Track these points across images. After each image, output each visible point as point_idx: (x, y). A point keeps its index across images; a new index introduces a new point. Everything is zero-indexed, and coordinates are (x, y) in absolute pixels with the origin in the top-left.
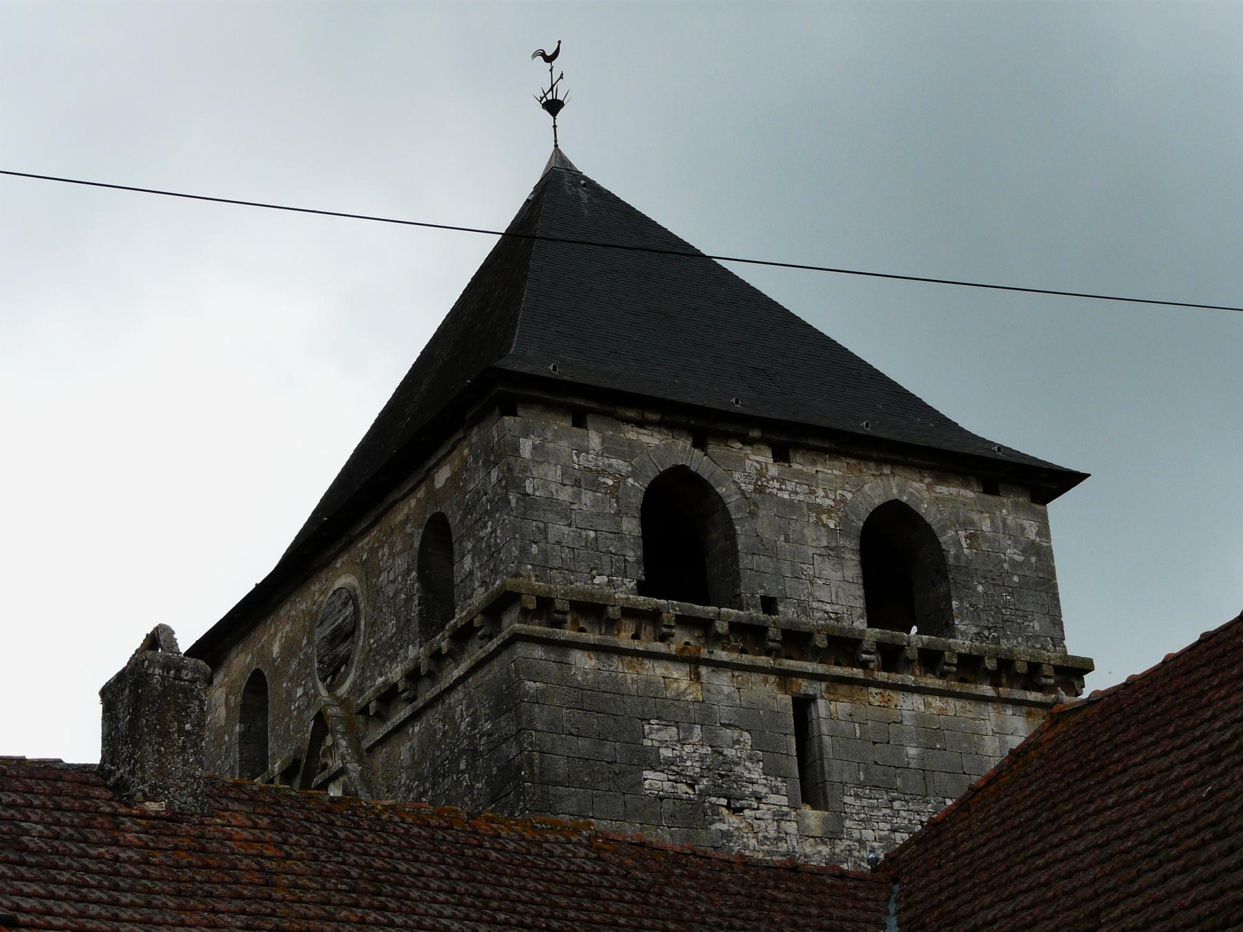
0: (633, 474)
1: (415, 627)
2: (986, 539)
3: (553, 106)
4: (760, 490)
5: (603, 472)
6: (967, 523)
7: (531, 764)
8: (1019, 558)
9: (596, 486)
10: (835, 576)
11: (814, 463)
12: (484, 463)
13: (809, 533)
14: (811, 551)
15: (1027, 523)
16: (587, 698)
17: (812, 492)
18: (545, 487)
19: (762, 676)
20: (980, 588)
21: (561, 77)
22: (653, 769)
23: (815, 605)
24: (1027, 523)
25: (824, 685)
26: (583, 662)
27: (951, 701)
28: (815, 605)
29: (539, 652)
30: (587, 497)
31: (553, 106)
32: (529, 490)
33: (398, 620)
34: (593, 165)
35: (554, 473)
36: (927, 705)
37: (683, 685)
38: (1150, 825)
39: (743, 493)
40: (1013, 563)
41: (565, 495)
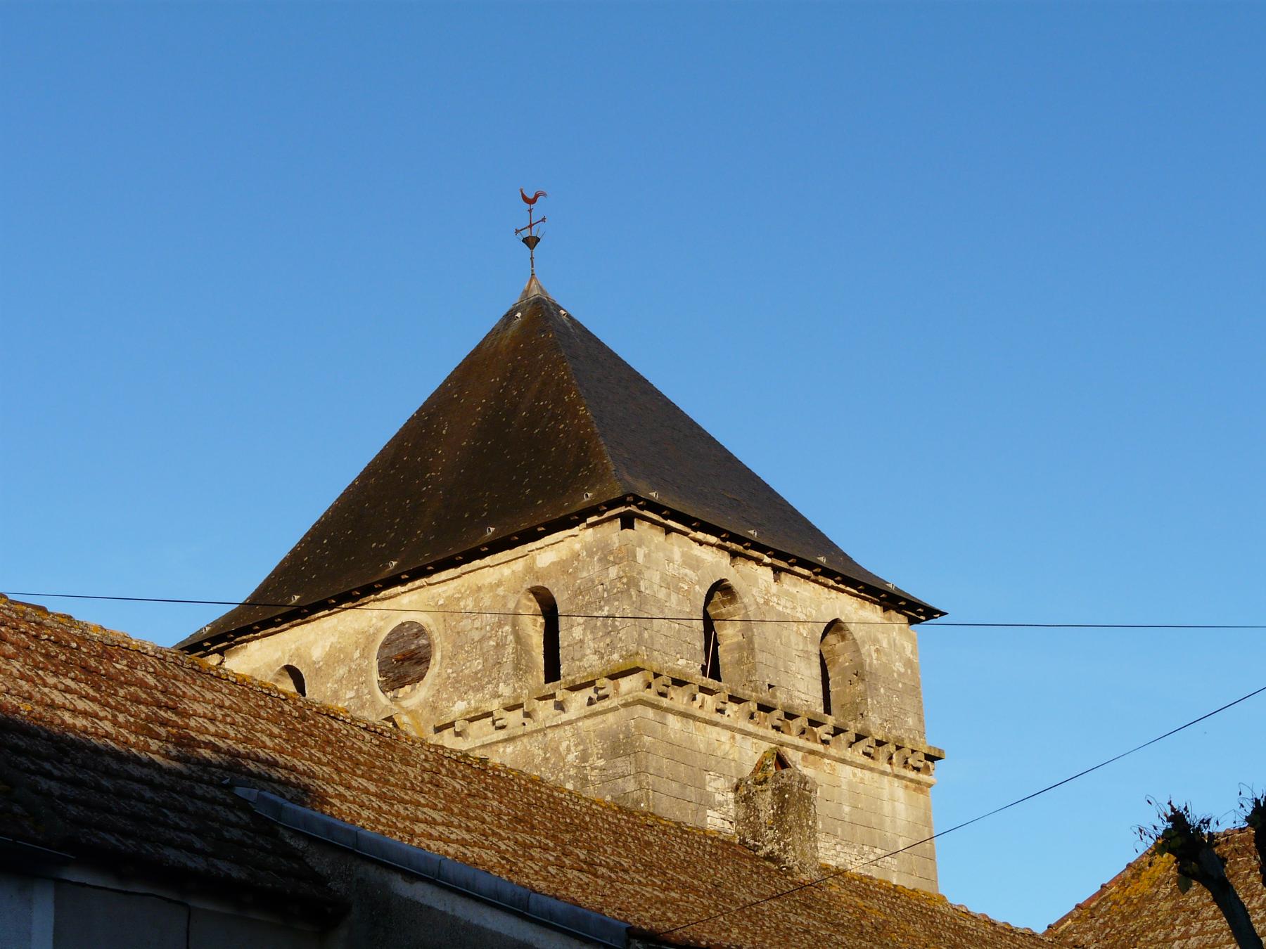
0: (699, 583)
1: (508, 669)
2: (886, 654)
3: (531, 242)
4: (767, 603)
5: (681, 579)
6: (875, 641)
7: (648, 799)
8: (902, 670)
9: (678, 590)
10: (807, 673)
11: (795, 585)
12: (600, 560)
13: (793, 639)
14: (794, 653)
15: (906, 644)
16: (679, 751)
17: (794, 608)
18: (651, 587)
19: (729, 733)
20: (882, 690)
21: (543, 220)
22: (712, 808)
23: (796, 693)
24: (906, 644)
25: (801, 754)
26: (673, 722)
27: (867, 773)
28: (796, 693)
29: (650, 713)
30: (674, 597)
31: (531, 242)
32: (642, 589)
33: (485, 660)
34: (584, 305)
35: (656, 578)
36: (854, 775)
37: (727, 747)
38: (216, 735)
39: (757, 604)
40: (900, 674)
41: (662, 594)
